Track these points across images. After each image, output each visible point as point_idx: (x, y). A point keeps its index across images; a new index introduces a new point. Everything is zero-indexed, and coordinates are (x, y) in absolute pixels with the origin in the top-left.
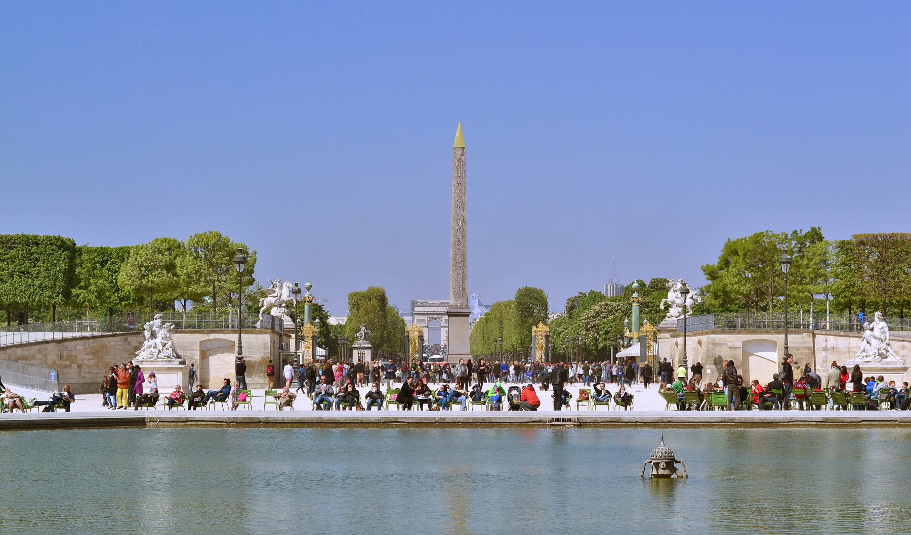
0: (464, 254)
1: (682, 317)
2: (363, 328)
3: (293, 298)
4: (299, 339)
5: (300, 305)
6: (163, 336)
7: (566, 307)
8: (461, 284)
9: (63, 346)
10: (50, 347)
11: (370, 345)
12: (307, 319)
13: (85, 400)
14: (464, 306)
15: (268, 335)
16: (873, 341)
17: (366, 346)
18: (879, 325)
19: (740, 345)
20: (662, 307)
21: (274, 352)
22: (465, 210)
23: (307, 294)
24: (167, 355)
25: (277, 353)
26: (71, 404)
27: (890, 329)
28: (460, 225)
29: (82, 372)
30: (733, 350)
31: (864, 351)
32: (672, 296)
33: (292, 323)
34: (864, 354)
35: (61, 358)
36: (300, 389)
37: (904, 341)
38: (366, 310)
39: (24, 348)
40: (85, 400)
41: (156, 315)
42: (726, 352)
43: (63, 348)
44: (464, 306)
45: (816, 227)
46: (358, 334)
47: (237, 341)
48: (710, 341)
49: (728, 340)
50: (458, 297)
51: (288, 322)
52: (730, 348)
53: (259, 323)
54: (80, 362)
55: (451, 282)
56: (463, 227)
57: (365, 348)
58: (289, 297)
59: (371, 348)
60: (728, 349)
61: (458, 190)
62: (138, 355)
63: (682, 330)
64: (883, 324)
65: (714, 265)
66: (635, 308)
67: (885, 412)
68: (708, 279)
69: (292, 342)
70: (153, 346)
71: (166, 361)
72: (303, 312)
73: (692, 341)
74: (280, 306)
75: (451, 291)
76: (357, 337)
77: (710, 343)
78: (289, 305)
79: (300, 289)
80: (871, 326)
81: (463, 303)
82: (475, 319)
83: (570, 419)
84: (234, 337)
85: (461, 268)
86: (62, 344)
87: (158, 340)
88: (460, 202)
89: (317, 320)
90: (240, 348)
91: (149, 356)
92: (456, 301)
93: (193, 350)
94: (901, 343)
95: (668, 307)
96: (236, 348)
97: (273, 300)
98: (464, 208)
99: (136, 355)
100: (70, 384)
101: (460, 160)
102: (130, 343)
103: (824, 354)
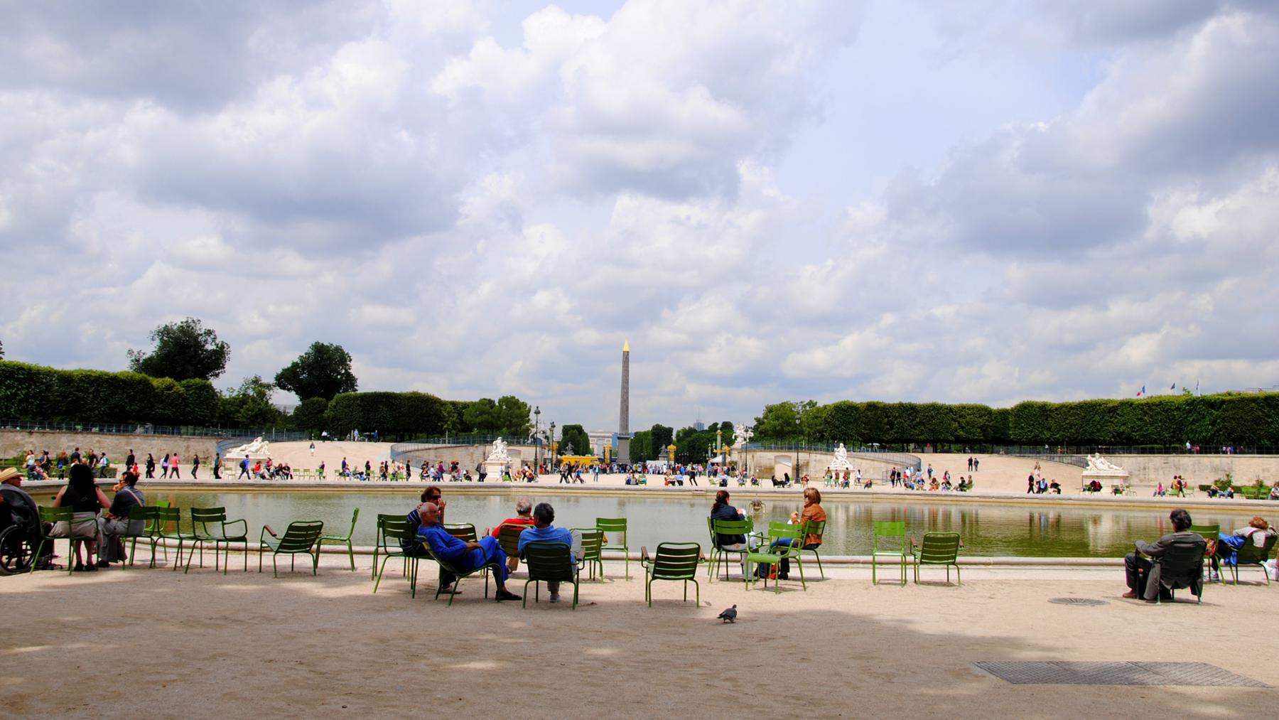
2: (570, 445)
7: (209, 333)
10: (431, 451)
13: (356, 513)
16: (839, 457)
19: (773, 457)
20: (733, 437)
27: (848, 451)
35: (436, 457)
36: (457, 590)
38: (433, 477)
40: (356, 513)
63: (745, 450)
64: (844, 449)
65: (263, 441)
66: (719, 438)
103: (815, 463)
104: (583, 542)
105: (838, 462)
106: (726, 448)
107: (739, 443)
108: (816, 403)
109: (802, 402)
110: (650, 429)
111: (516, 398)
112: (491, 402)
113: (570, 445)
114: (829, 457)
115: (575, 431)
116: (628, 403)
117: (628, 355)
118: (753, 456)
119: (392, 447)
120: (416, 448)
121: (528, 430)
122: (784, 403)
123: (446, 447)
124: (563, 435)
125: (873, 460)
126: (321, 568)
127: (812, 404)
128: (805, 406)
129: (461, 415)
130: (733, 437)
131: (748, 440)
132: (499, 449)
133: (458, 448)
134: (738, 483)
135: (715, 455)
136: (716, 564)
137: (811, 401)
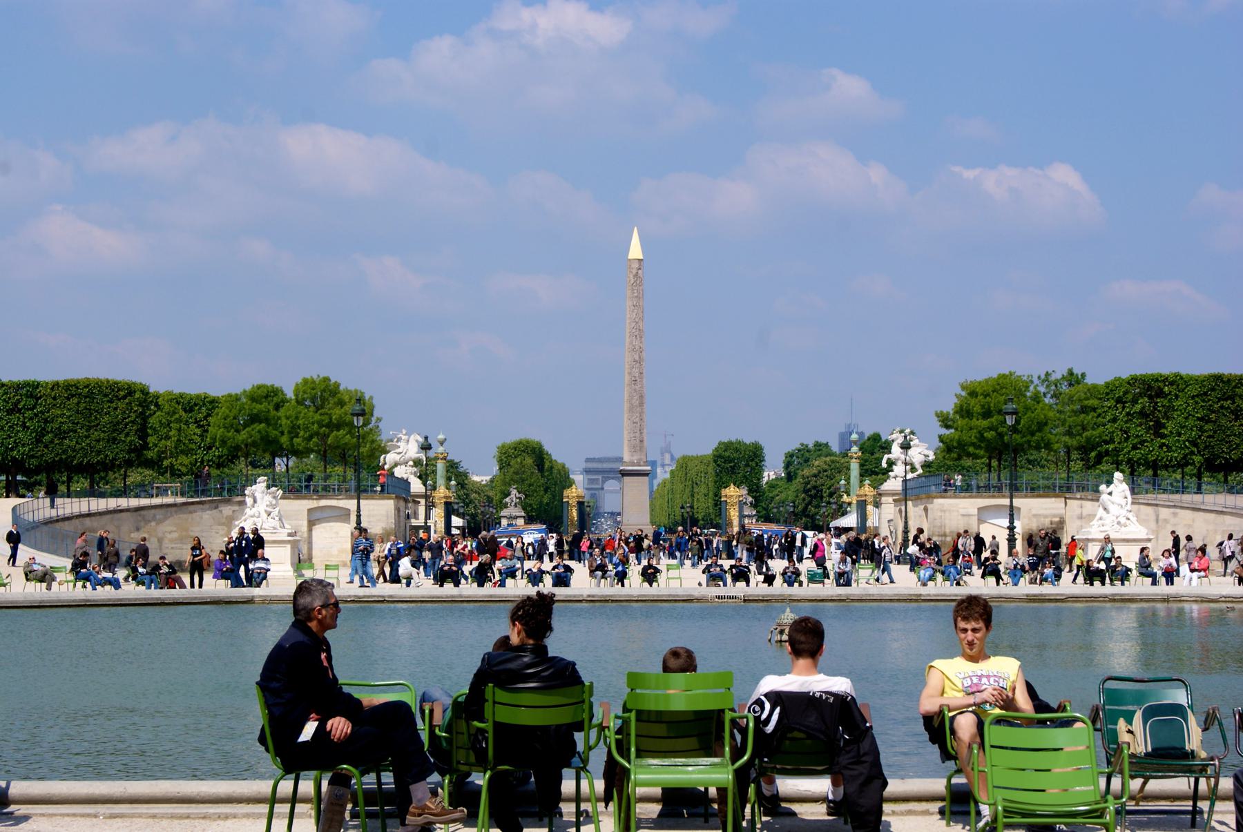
0: (641, 397)
2: (514, 492)
3: (422, 456)
4: (430, 506)
5: (431, 462)
8: (638, 435)
11: (523, 514)
12: (441, 481)
14: (642, 463)
15: (392, 502)
16: (1111, 507)
17: (518, 514)
18: (1119, 488)
19: (975, 512)
20: (884, 465)
21: (399, 522)
23: (441, 449)
25: (402, 524)
28: (637, 358)
30: (966, 518)
31: (1101, 519)
32: (896, 451)
33: (422, 486)
34: (1100, 522)
37: (1175, 506)
39: (93, 518)
43: (140, 518)
44: (642, 463)
46: (507, 500)
49: (961, 506)
51: (417, 486)
52: (963, 515)
54: (160, 535)
55: (626, 432)
56: (639, 361)
57: (516, 517)
58: (418, 453)
59: (524, 517)
60: (960, 517)
61: (634, 314)
67: (904, 580)
69: (422, 510)
71: (272, 533)
72: (434, 472)
74: (406, 463)
75: (626, 443)
76: (507, 503)
78: (417, 463)
79: (430, 445)
80: (1109, 490)
81: (641, 459)
84: (351, 504)
85: (638, 415)
86: (139, 512)
89: (453, 482)
90: (359, 516)
92: (632, 456)
94: (1172, 510)
95: (891, 463)
96: (353, 518)
97: (397, 458)
98: (641, 337)
100: (823, 692)
101: (636, 275)
103: (1078, 523)
105: (1109, 518)
107: (893, 484)
108: (1083, 375)
111: (300, 381)
114: (1088, 506)
118: (926, 510)
119: (14, 509)
120: (85, 509)
125: (1222, 513)
126: (311, 780)
127: (1073, 379)
130: (884, 465)
131: (920, 471)
132: (261, 507)
134: (703, 578)
135: (842, 511)
136: (286, 808)
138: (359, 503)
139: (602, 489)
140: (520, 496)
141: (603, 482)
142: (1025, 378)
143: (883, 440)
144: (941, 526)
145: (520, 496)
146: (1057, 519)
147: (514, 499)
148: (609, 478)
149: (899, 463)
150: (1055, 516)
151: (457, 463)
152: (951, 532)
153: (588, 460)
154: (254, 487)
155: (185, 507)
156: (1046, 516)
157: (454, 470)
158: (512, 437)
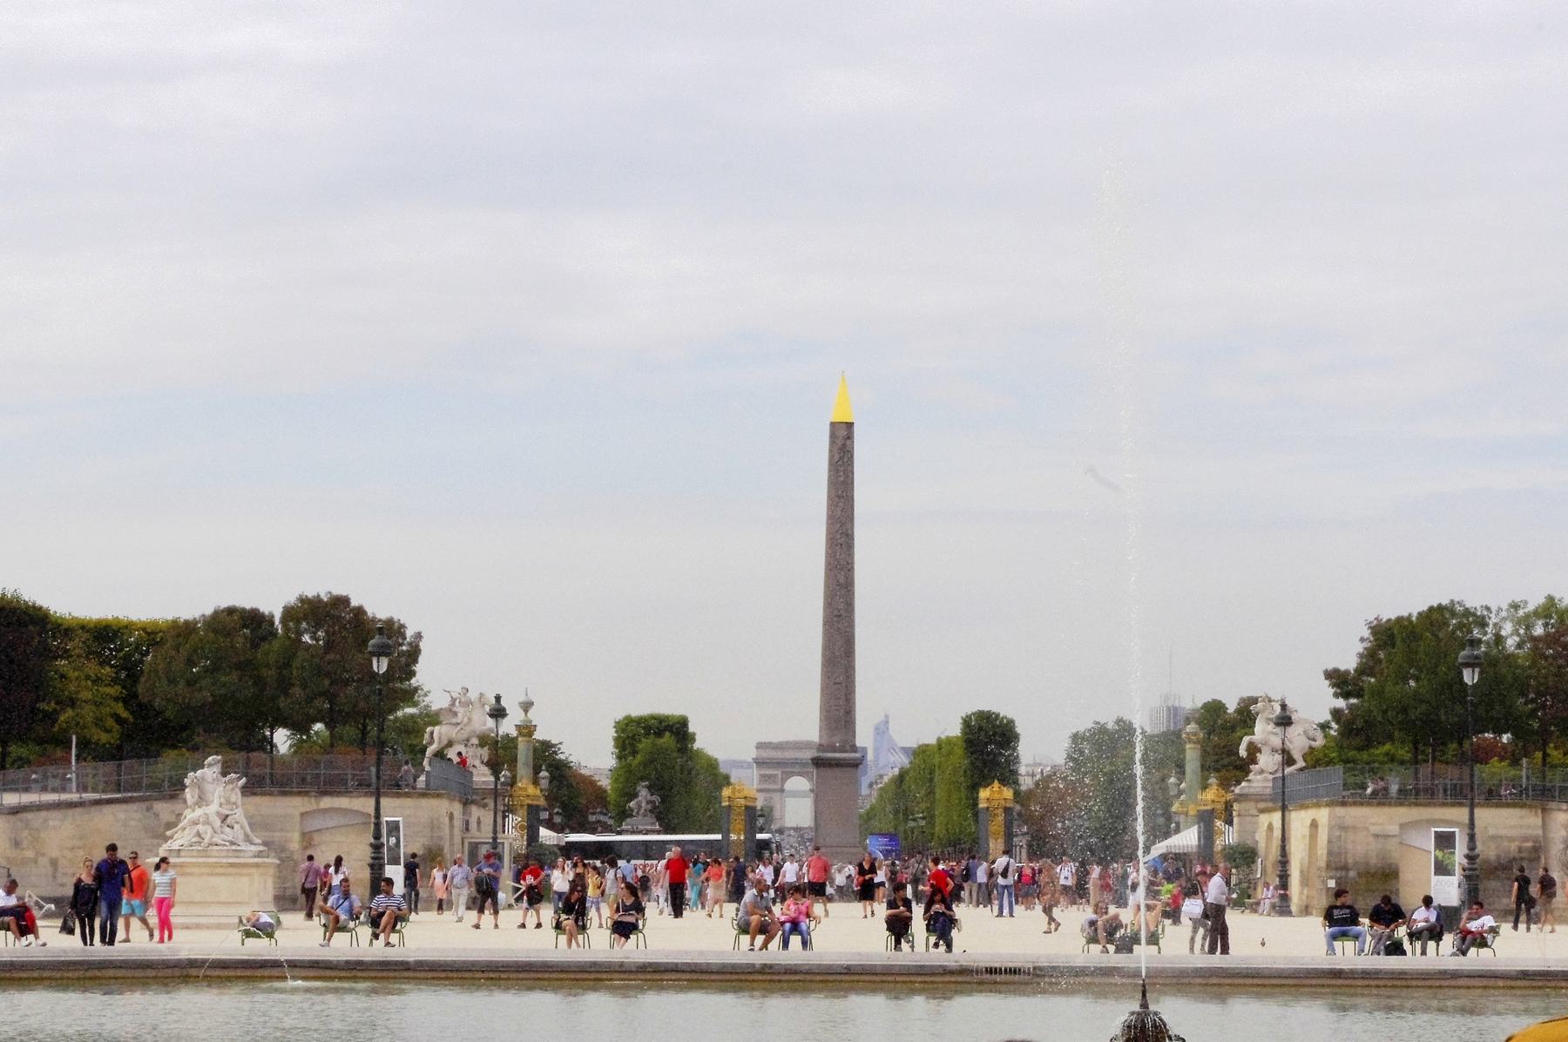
1: (1279, 774)
2: (643, 793)
6: (223, 800)
9: (21, 821)
12: (524, 771)
20: (1243, 752)
22: (473, 695)
24: (230, 838)
26: (421, 643)
28: (842, 580)
29: (59, 875)
41: (210, 758)
42: (1368, 844)
43: (19, 824)
45: (1510, 601)
46: (632, 804)
47: (371, 811)
48: (1333, 823)
50: (837, 728)
52: (1376, 836)
53: (423, 778)
60: (1371, 839)
62: (171, 837)
68: (1336, 695)
70: (201, 820)
73: (1300, 820)
77: (1334, 826)
79: (504, 709)
82: (881, 777)
83: (1020, 970)
86: (20, 816)
87: (213, 809)
88: (841, 534)
91: (194, 840)
92: (833, 735)
93: (287, 832)
95: (1254, 750)
99: (166, 839)
102: (157, 815)
104: (1222, 953)
106: (1212, 795)
107: (1259, 780)
109: (1515, 606)
110: (955, 730)
112: (254, 620)
113: (643, 793)
115: (667, 740)
116: (851, 625)
117: (850, 437)
121: (413, 729)
122: (1440, 608)
123: (57, 806)
124: (620, 757)
128: (1527, 621)
129: (130, 671)
130: (1243, 752)
133: (108, 809)
137: (1551, 599)
138: (378, 803)
139: (782, 790)
140: (653, 798)
141: (784, 781)
142: (205, 984)
143: (1333, 690)
144: (1340, 854)
145: (653, 798)
146: (1529, 844)
147: (643, 805)
148: (793, 774)
149: (1266, 750)
150: (1526, 839)
151: (554, 746)
152: (1356, 863)
153: (760, 746)
154: (199, 772)
155: (98, 807)
156: (1511, 839)
157: (545, 755)
158: (642, 707)
